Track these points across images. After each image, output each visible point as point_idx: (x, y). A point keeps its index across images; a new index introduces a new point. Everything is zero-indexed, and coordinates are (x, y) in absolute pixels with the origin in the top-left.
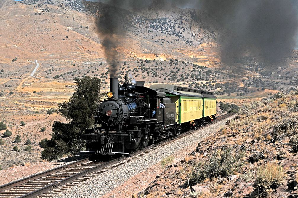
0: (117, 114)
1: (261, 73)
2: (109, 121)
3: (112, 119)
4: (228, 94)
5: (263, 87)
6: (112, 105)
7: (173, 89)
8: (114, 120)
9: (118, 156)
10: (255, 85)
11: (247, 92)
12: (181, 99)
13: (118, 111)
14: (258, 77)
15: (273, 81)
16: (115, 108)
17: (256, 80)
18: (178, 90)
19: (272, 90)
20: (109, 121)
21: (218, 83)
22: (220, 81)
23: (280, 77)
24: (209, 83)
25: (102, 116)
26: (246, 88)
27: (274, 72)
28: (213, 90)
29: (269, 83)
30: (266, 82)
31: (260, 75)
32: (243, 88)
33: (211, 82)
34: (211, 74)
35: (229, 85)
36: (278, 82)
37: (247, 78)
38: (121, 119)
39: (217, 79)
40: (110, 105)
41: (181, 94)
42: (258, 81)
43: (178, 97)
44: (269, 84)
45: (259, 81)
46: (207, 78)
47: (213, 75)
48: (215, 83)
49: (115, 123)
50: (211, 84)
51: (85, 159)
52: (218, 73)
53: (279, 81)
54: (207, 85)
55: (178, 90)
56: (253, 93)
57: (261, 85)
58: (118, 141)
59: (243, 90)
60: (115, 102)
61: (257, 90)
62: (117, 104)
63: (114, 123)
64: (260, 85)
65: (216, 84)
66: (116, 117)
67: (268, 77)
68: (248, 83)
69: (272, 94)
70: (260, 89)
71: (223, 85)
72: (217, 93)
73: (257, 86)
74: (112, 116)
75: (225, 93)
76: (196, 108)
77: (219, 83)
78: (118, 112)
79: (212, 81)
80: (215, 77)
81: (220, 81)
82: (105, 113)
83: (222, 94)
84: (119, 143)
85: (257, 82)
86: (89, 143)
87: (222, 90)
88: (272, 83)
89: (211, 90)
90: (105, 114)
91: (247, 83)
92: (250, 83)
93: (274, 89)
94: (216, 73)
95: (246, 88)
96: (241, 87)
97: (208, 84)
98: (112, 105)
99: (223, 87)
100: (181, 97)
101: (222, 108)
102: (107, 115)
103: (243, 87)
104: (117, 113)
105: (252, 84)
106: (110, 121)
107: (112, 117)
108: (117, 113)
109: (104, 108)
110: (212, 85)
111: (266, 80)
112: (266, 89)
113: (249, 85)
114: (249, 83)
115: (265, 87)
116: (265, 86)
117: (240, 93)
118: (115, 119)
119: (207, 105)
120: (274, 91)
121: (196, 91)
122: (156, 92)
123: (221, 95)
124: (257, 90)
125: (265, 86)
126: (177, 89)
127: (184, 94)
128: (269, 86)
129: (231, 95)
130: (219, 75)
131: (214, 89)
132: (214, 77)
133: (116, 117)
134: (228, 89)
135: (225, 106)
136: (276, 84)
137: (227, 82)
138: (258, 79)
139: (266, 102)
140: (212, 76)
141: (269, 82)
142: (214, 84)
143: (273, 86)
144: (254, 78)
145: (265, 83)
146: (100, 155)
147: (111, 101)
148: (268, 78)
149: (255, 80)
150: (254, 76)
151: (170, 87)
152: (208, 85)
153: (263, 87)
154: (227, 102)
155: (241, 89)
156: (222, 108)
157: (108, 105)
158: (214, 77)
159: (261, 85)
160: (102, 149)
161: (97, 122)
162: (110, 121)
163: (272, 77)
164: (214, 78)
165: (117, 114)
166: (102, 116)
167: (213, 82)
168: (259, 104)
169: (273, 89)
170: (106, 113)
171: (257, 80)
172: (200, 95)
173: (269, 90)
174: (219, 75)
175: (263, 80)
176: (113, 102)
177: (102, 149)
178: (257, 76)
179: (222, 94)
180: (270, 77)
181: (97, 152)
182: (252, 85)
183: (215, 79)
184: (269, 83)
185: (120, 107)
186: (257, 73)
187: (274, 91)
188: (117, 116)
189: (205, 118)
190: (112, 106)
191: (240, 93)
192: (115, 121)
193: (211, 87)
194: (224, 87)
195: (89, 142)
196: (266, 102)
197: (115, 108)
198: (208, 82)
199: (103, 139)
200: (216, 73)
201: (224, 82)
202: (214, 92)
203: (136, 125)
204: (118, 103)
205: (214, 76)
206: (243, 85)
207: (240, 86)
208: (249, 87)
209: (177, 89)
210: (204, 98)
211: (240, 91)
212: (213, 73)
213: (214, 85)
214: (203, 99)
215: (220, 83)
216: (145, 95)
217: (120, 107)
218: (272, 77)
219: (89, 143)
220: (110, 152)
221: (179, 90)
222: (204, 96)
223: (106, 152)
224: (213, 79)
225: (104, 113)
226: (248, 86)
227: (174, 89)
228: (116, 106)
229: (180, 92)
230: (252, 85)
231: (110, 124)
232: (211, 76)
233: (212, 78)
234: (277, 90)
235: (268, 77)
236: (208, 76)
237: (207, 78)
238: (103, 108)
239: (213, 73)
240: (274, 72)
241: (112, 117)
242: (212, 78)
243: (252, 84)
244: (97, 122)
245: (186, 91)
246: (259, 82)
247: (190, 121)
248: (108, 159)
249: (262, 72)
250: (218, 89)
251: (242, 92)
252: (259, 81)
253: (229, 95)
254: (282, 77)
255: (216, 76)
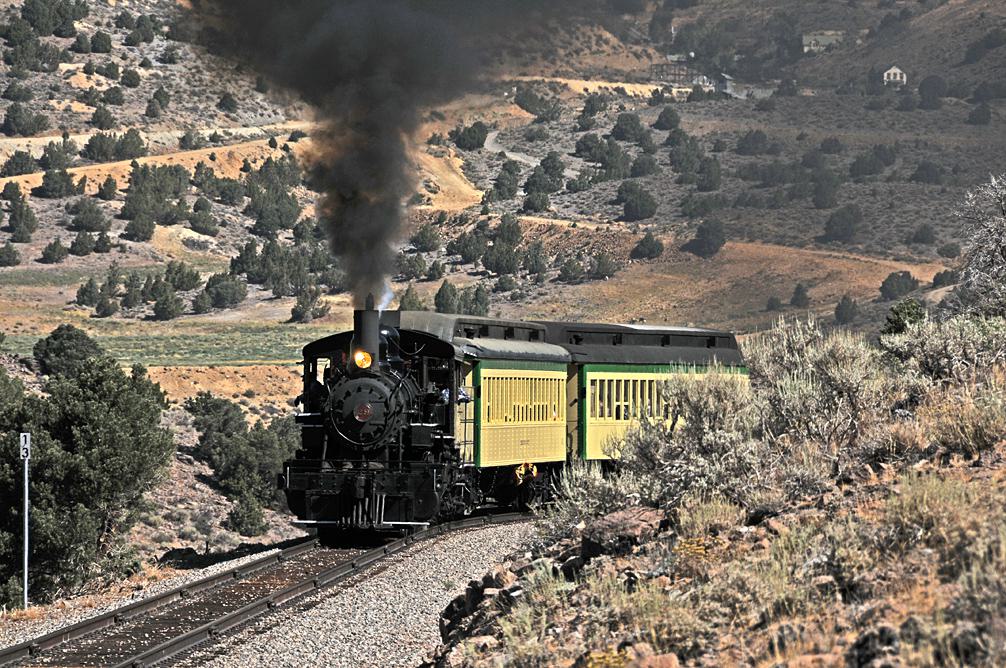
0: (386, 415)
1: (679, 45)
3: (371, 430)
4: (292, 303)
5: (703, 208)
6: (372, 390)
7: (451, 332)
8: (375, 433)
9: (396, 533)
10: (610, 188)
11: (521, 279)
12: (484, 372)
13: (387, 405)
14: (646, 90)
15: (817, 135)
17: (619, 133)
18: (468, 337)
19: (808, 252)
21: (161, 161)
22: (185, 144)
23: (904, 89)
24: (43, 164)
26: (508, 232)
27: (831, 36)
28: (103, 246)
29: (769, 160)
30: (741, 150)
31: (658, 72)
32: (469, 228)
33: (69, 148)
34: (76, 48)
36: (883, 156)
37: (515, 110)
39: (151, 113)
40: (363, 390)
41: (482, 350)
42: (642, 139)
43: (474, 364)
44: (768, 178)
45: (660, 136)
46: (26, 95)
47: (97, 59)
48: (125, 166)
50: (78, 173)
51: (300, 545)
52: (159, 44)
53: (889, 138)
54: (25, 190)
55: (470, 335)
56: (584, 289)
58: (399, 489)
59: (463, 251)
61: (636, 254)
64: (661, 186)
65: (139, 176)
66: (383, 423)
67: (761, 94)
69: (811, 293)
70: (667, 240)
71: (228, 193)
72: (153, 291)
73: (633, 208)
74: (372, 422)
75: (253, 291)
76: (541, 413)
77: (177, 171)
78: (388, 409)
79: (81, 140)
80: (128, 92)
81: (185, 144)
82: (352, 413)
83: (219, 302)
85: (633, 152)
86: (314, 497)
87: (218, 256)
88: (810, 161)
89: (78, 249)
90: (352, 416)
91: (511, 167)
92: (551, 165)
93: (839, 234)
94: (130, 42)
95: (508, 232)
96: (441, 217)
97: (37, 179)
98: (372, 390)
100: (483, 361)
101: (229, 473)
102: (357, 418)
103: (462, 220)
109: (348, 398)
110: (92, 189)
111: (744, 127)
112: (738, 233)
113: (541, 187)
114: (535, 163)
115: (727, 220)
117: (437, 286)
118: (379, 430)
119: (514, 403)
120: (831, 265)
121: (541, 334)
123: (198, 310)
124: (636, 254)
125: (722, 202)
126: (466, 330)
127: (493, 352)
128: (773, 204)
129: (321, 314)
130: (168, 58)
131: (113, 235)
132: (105, 84)
133: (383, 423)
134: (284, 237)
136: (858, 171)
137: (277, 154)
138: (646, 121)
139: (943, 353)
140: (81, 82)
141: (774, 151)
142: (110, 183)
143: (819, 206)
144: (593, 104)
145: (728, 161)
147: (364, 379)
148: (763, 106)
150: (593, 86)
151: (440, 325)
152: (37, 193)
153: (703, 208)
155: (445, 235)
157: (359, 389)
158: (105, 84)
163: (808, 92)
164: (114, 97)
165: (386, 415)
167: (96, 152)
168: (854, 375)
169: (821, 241)
171: (626, 128)
172: (560, 351)
173: (771, 250)
174: (168, 58)
175: (698, 126)
176: (374, 382)
178: (629, 79)
179: (220, 296)
180: (787, 90)
181: (341, 521)
183: (132, 111)
184: (769, 160)
185: (393, 396)
186: (623, 38)
187: (834, 260)
190: (370, 392)
191: (437, 286)
192: (379, 434)
193: (70, 210)
194: (236, 218)
195: (312, 495)
196: (943, 353)
198: (38, 154)
199: (363, 485)
200: (130, 42)
201: (242, 150)
202: (112, 283)
204: (386, 385)
205: (110, 72)
207: (435, 207)
208: (537, 220)
209: (466, 330)
210: (586, 366)
211: (428, 259)
212: (100, 44)
213: (107, 191)
214: (576, 369)
215: (188, 160)
217: (393, 396)
218: (808, 92)
219: (314, 497)
220: (379, 522)
221: (473, 334)
224: (100, 120)
225: (347, 413)
226: (529, 207)
227: (457, 333)
228: (382, 393)
229: (476, 341)
230: (573, 187)
232: (75, 73)
233: (78, 107)
234: (867, 252)
235: (761, 94)
236: (34, 80)
237: (26, 95)
239: (100, 44)
240: (831, 36)
242: (87, 97)
244: (326, 438)
246: (661, 156)
247: (513, 468)
248: (375, 540)
249: (688, 27)
250: (169, 240)
251: (462, 279)
252: (660, 136)
254: (928, 93)
255: (131, 80)
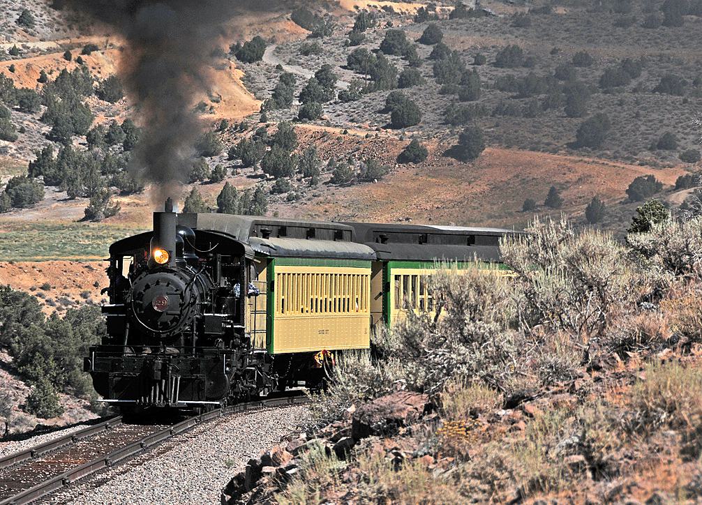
0: (181, 305)
2: (159, 324)
3: (167, 319)
5: (465, 116)
6: (169, 284)
9: (192, 412)
10: (379, 98)
11: (293, 182)
12: (277, 269)
13: (182, 297)
15: (569, 50)
16: (176, 291)
17: (387, 48)
18: (263, 237)
20: (159, 324)
25: (142, 312)
26: (285, 139)
29: (525, 72)
30: (498, 64)
32: (248, 135)
35: (92, 101)
36: (630, 68)
38: (190, 318)
40: (161, 284)
42: (408, 54)
43: (266, 261)
44: (525, 89)
45: (424, 51)
49: (175, 329)
53: (635, 54)
55: (266, 235)
57: (446, 100)
58: (192, 372)
59: (242, 155)
60: (175, 275)
61: (402, 159)
62: (181, 281)
63: (172, 331)
68: (305, 74)
70: (431, 146)
73: (400, 117)
74: (169, 312)
75: (50, 193)
78: (183, 301)
84: (195, 379)
86: (117, 378)
90: (151, 306)
91: (287, 79)
92: (324, 77)
95: (285, 139)
96: (223, 125)
98: (169, 284)
99: (27, 120)
101: (27, 360)
102: (155, 308)
103: (243, 127)
104: (180, 304)
105: (342, 85)
106: (162, 324)
107: (167, 314)
108: (180, 304)
111: (501, 42)
112: (496, 139)
114: (310, 75)
115: (484, 126)
116: (482, 112)
117: (219, 188)
118: (175, 320)
122: (244, 247)
124: (402, 159)
125: (482, 112)
127: (288, 251)
128: (529, 114)
129: (113, 213)
135: (56, 333)
136: (609, 82)
138: (412, 36)
141: (528, 64)
143: (571, 114)
146: (154, 408)
149: (372, 43)
153: (465, 116)
154: (74, 295)
155: (227, 142)
156: (27, 360)
157: (158, 283)
159: (446, 100)
160: (152, 394)
161: (128, 326)
162: (162, 324)
165: (181, 305)
166: (142, 312)
168: (603, 270)
169: (572, 147)
170: (153, 304)
172: (365, 249)
173: (527, 155)
176: (171, 276)
177: (152, 394)
181: (140, 401)
182: (344, 98)
184: (525, 72)
185: (188, 289)
187: (584, 164)
188: (181, 311)
189: (277, 356)
190: (167, 286)
191: (219, 188)
192: (175, 323)
197: (176, 291)
201: (40, 63)
203: (220, 337)
206: (247, 98)
207: (216, 116)
208: (311, 127)
210: (390, 263)
211: (211, 163)
216: (211, 255)
217: (188, 289)
219: (117, 378)
220: (174, 401)
222: (384, 256)
223: (166, 399)
226: (304, 116)
227: (252, 233)
230: (344, 98)
231: (163, 333)
238: (144, 291)
241: (167, 314)
243: (342, 85)
245: (297, 237)
246: (425, 69)
248: (172, 417)
252: (424, 51)
253: (90, 215)
